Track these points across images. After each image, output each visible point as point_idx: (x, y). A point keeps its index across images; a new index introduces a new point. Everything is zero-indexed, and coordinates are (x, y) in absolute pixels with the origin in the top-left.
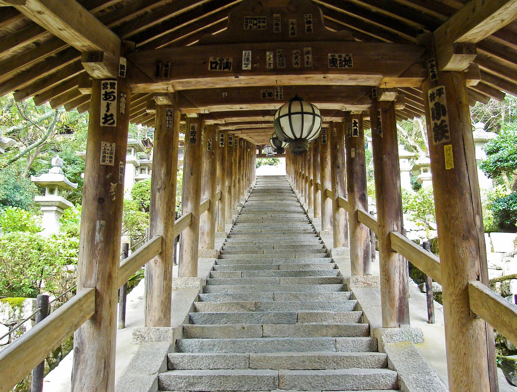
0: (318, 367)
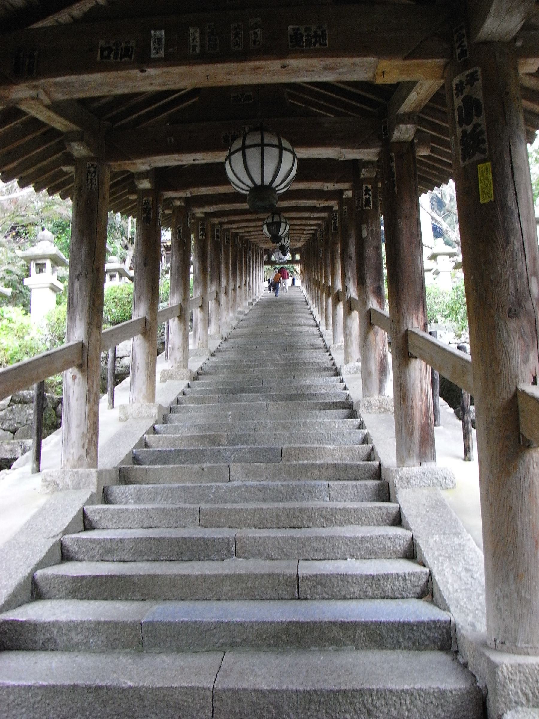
0: (299, 524)
